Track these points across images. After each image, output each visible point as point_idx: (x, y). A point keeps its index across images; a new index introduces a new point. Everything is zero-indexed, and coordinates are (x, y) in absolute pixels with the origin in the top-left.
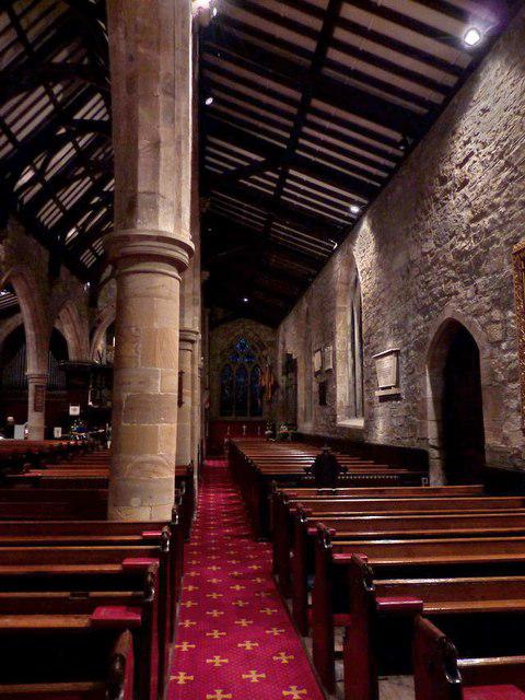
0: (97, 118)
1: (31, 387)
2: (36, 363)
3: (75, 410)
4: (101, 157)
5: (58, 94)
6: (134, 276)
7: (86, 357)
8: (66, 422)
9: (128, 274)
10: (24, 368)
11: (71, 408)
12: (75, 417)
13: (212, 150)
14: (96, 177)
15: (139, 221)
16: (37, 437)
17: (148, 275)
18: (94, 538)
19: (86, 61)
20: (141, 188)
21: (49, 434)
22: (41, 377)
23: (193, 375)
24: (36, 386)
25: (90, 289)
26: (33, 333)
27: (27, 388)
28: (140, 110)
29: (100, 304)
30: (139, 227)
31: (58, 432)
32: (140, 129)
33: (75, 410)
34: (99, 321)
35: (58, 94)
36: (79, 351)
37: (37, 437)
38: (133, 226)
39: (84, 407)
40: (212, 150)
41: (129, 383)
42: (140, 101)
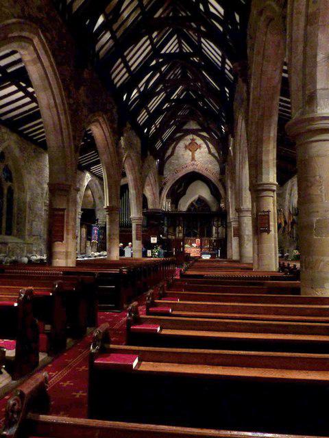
0: (173, 51)
1: (134, 226)
2: (136, 211)
3: (154, 240)
4: (172, 77)
5: (186, 14)
6: (314, 144)
7: (158, 207)
8: (152, 246)
9: (307, 143)
10: (129, 214)
11: (152, 238)
12: (154, 244)
13: (27, 132)
14: (168, 91)
15: (318, 108)
16: (138, 255)
17: (320, 143)
18: (261, 316)
19: (171, 14)
20: (319, 86)
21: (145, 254)
22: (140, 219)
23: (274, 213)
24: (137, 225)
25: (159, 164)
26: (134, 192)
27: (131, 226)
28: (320, 36)
29: (165, 173)
30: (319, 112)
31: (149, 253)
32: (319, 48)
33: (154, 240)
34: (165, 184)
35: (186, 14)
36: (154, 202)
37: (138, 255)
38: (313, 111)
39: (159, 239)
40: (27, 132)
41: (318, 212)
42: (321, 29)
